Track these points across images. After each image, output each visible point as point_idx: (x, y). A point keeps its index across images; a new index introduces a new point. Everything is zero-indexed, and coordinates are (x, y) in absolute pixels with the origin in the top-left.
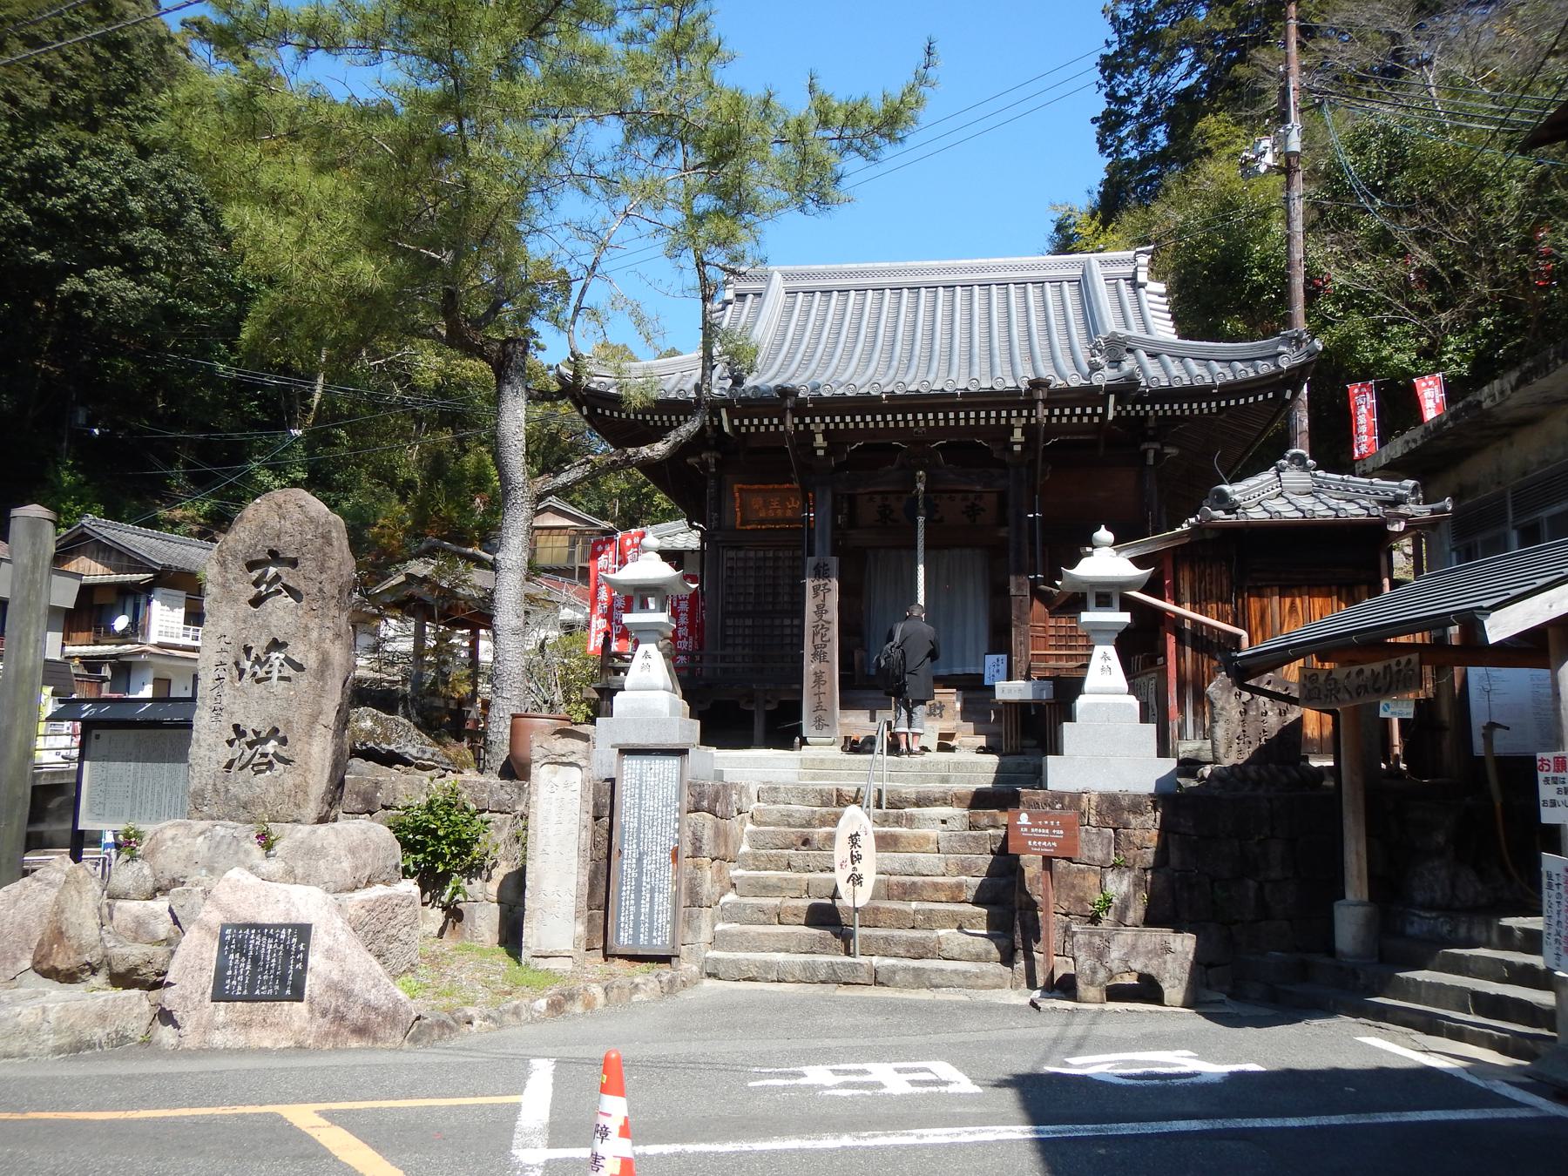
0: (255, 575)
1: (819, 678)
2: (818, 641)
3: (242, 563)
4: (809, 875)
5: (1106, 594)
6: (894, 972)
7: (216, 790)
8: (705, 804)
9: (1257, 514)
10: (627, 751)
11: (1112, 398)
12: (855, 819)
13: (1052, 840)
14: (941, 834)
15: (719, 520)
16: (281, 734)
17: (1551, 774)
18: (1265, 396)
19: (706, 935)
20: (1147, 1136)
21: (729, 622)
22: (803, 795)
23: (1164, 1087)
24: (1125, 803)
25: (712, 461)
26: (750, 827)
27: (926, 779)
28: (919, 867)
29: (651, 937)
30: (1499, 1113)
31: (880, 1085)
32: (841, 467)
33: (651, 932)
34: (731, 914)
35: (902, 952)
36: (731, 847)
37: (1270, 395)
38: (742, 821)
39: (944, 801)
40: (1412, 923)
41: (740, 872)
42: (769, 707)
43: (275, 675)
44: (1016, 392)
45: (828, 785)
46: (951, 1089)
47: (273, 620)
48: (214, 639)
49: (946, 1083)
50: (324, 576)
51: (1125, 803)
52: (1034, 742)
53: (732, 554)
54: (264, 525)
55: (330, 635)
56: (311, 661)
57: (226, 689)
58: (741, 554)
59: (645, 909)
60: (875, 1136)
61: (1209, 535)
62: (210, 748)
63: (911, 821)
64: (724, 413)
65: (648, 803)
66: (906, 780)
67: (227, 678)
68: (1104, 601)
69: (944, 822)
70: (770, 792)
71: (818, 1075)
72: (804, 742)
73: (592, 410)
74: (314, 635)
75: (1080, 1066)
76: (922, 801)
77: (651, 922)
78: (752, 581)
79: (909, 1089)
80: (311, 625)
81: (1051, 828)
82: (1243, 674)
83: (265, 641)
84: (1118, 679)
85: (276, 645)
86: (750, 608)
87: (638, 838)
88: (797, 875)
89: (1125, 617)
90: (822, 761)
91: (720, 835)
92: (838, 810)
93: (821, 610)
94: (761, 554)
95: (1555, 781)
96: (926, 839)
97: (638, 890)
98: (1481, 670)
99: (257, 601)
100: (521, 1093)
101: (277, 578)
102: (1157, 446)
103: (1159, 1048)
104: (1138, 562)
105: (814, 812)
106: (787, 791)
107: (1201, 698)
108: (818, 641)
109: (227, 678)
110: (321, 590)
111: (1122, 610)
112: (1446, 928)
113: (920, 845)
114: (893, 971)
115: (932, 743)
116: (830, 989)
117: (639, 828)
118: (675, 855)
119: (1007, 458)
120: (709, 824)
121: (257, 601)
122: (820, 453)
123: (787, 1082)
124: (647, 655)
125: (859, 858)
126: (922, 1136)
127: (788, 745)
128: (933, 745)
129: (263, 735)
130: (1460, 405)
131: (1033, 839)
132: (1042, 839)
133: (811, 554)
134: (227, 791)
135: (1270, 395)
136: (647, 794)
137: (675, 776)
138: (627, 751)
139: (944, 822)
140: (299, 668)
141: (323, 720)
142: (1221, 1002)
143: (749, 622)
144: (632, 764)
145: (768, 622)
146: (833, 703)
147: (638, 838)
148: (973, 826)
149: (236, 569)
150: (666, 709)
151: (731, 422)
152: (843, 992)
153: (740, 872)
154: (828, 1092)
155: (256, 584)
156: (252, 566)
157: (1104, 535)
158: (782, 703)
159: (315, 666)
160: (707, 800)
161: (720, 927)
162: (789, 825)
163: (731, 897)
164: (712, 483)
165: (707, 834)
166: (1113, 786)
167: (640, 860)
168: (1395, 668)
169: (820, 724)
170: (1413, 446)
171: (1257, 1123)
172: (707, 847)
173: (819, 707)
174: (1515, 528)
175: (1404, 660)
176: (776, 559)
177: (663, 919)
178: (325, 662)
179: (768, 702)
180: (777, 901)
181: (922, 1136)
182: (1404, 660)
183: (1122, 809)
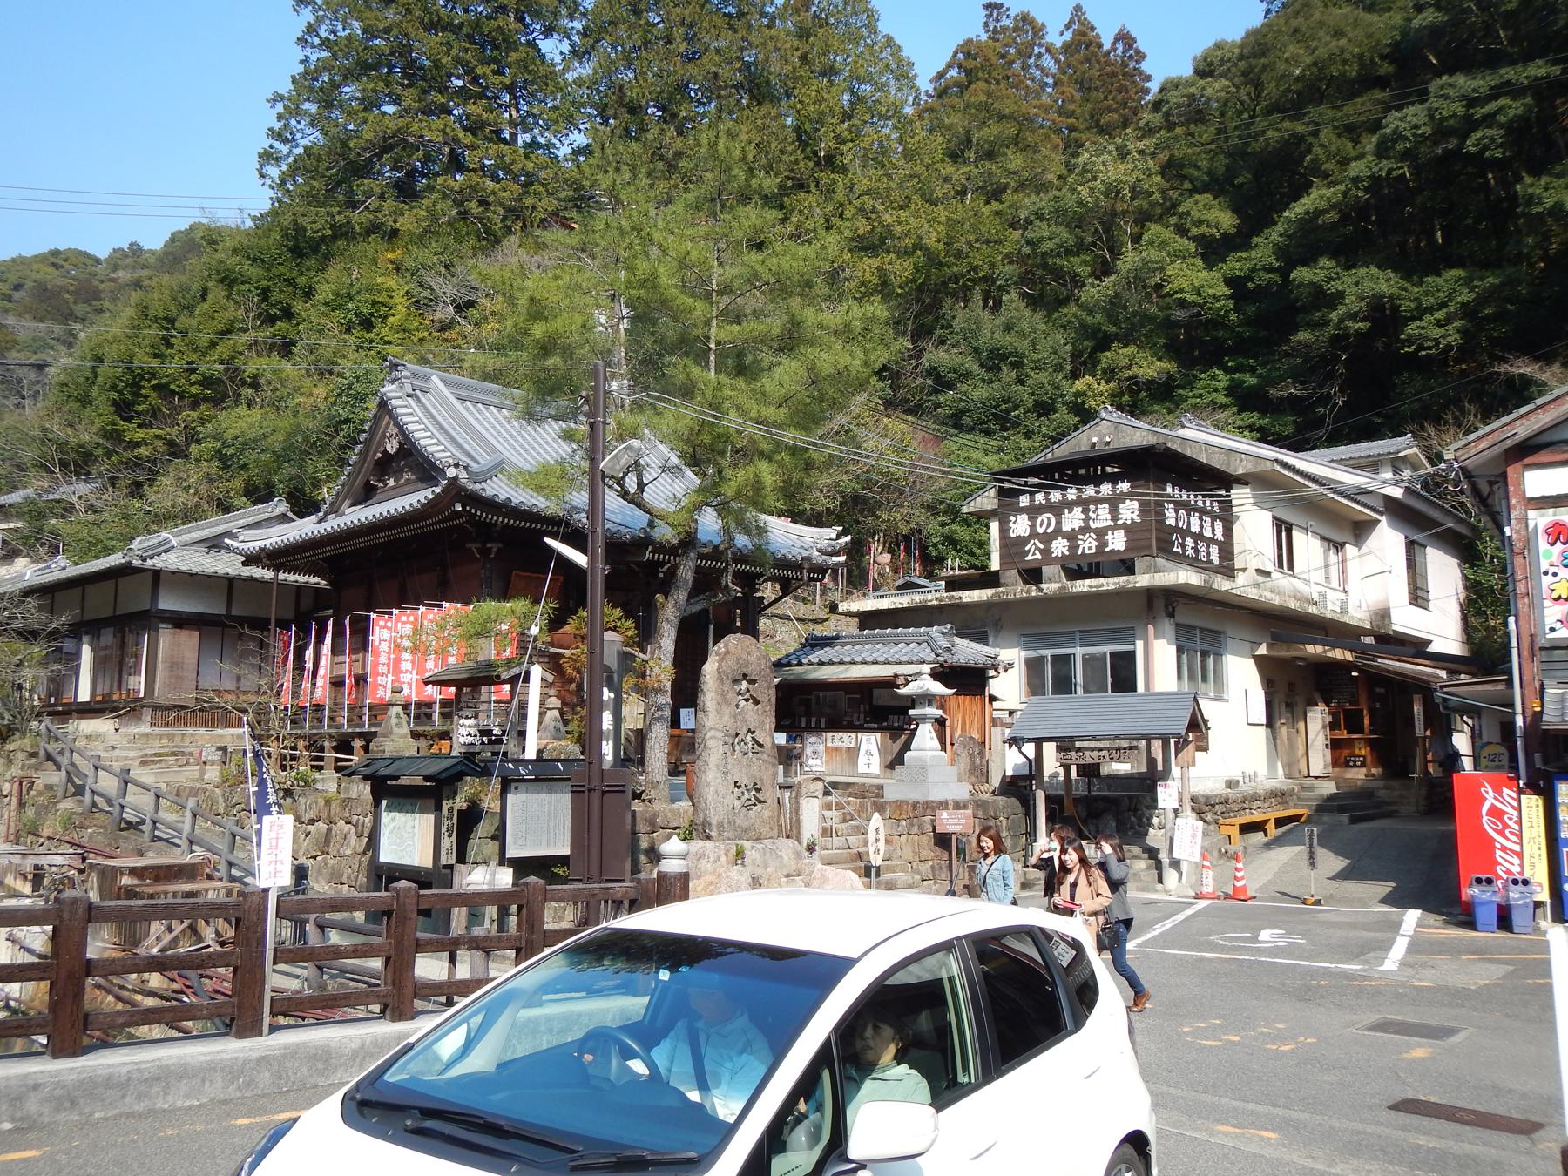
140: (761, 745)
149: (728, 683)
156: (735, 682)
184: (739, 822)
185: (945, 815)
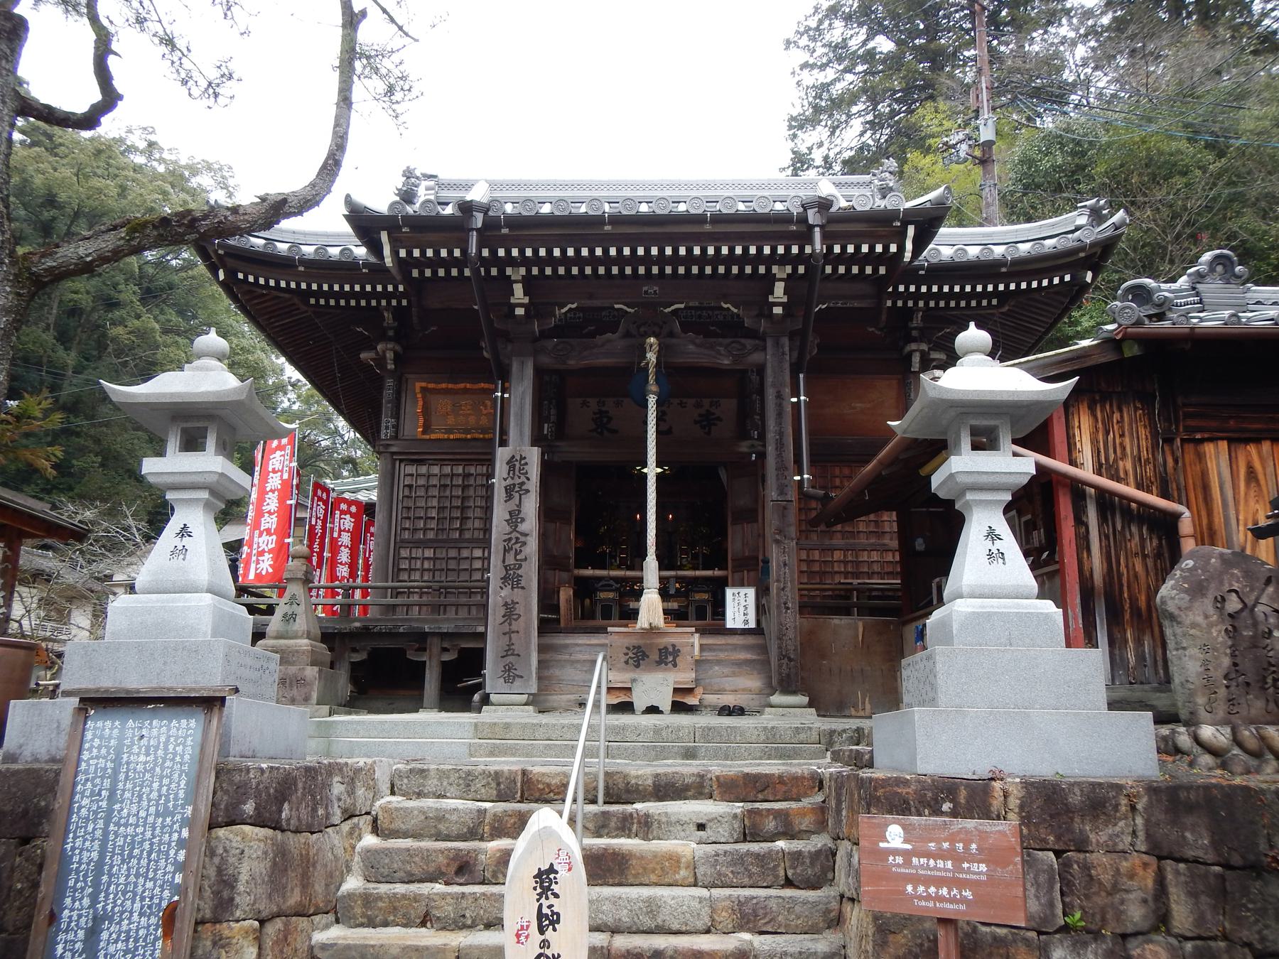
1: (510, 610)
2: (510, 560)
5: (985, 422)
10: (101, 702)
11: (911, 230)
12: (552, 834)
13: (961, 884)
15: (396, 427)
18: (1062, 279)
21: (404, 553)
22: (467, 783)
24: (1076, 799)
25: (390, 355)
27: (661, 754)
28: (664, 917)
32: (545, 335)
36: (319, 888)
37: (1067, 278)
38: (355, 834)
39: (697, 789)
42: (447, 657)
44: (784, 218)
45: (508, 764)
51: (1076, 799)
52: (805, 700)
53: (411, 469)
58: (423, 470)
61: (1131, 351)
63: (645, 826)
64: (384, 236)
65: (126, 809)
66: (632, 756)
68: (984, 441)
69: (701, 827)
70: (412, 780)
72: (486, 700)
73: (231, 274)
76: (666, 790)
78: (435, 503)
84: (1018, 571)
86: (431, 535)
87: (96, 884)
90: (507, 726)
92: (523, 807)
93: (515, 518)
94: (447, 470)
100: (515, 838)
102: (924, 347)
105: (482, 812)
106: (443, 775)
108: (510, 560)
113: (664, 871)
117: (100, 864)
118: (170, 918)
119: (763, 325)
122: (520, 311)
124: (184, 532)
125: (554, 920)
127: (466, 706)
128: (666, 705)
131: (916, 880)
132: (939, 882)
133: (503, 443)
135: (1067, 278)
138: (101, 702)
139: (701, 827)
143: (429, 553)
145: (453, 553)
146: (528, 643)
147: (96, 884)
148: (748, 835)
150: (205, 625)
151: (395, 253)
157: (972, 325)
158: (462, 651)
162: (439, 837)
164: (390, 382)
166: (1044, 768)
167: (93, 934)
169: (510, 674)
173: (509, 651)
176: (466, 476)
179: (445, 650)
183: (1069, 810)
185: (895, 836)
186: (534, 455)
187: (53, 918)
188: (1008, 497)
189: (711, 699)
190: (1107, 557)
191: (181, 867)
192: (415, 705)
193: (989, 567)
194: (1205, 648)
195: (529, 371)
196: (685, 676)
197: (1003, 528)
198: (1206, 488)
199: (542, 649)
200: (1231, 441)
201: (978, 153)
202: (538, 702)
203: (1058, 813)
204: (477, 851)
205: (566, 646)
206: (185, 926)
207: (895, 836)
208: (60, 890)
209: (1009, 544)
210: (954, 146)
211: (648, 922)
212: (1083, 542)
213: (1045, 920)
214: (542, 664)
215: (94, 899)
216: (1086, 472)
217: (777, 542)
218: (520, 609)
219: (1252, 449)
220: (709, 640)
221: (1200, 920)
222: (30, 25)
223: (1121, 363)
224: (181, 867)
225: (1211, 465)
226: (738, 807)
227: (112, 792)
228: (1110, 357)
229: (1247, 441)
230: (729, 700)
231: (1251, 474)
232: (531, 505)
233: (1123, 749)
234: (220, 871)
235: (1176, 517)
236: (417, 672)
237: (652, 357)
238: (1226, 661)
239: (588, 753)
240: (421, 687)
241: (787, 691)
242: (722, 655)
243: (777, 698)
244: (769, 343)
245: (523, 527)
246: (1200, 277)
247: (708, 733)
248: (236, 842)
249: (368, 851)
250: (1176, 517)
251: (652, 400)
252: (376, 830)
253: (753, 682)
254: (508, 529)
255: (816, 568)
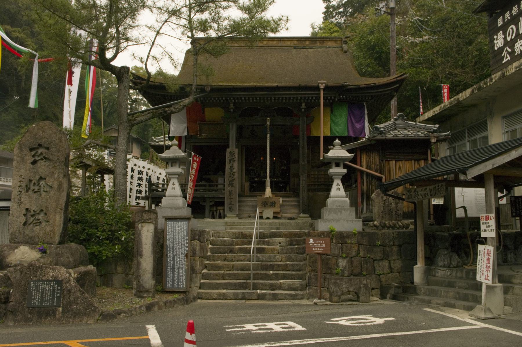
0: (33, 153)
1: (231, 193)
2: (231, 179)
3: (28, 149)
4: (232, 263)
6: (266, 295)
7: (20, 233)
8: (197, 237)
9: (390, 135)
10: (168, 219)
13: (321, 248)
14: (279, 248)
16: (44, 212)
17: (484, 221)
19: (198, 285)
20: (363, 339)
23: (365, 326)
26: (210, 246)
27: (272, 229)
29: (178, 285)
30: (469, 327)
31: (271, 329)
33: (178, 283)
34: (205, 276)
35: (268, 288)
40: (438, 272)
41: (207, 262)
43: (42, 190)
46: (296, 329)
47: (40, 170)
48: (18, 177)
49: (294, 328)
50: (60, 154)
52: (308, 215)
54: (36, 135)
55: (62, 175)
56: (56, 185)
57: (23, 196)
59: (176, 275)
60: (275, 343)
61: (373, 142)
62: (17, 217)
63: (268, 243)
67: (23, 191)
68: (337, 165)
69: (280, 243)
71: (249, 327)
74: (56, 175)
75: (336, 321)
77: (178, 280)
79: (282, 330)
80: (55, 172)
81: (321, 244)
82: (385, 189)
83: (37, 177)
85: (41, 178)
87: (173, 250)
88: (229, 263)
89: (345, 171)
90: (234, 222)
91: (202, 248)
93: (232, 168)
95: (486, 223)
96: (274, 249)
97: (173, 269)
98: (460, 189)
99: (34, 163)
101: (41, 154)
103: (360, 314)
104: (349, 151)
107: (369, 198)
108: (231, 179)
109: (23, 191)
110: (58, 159)
111: (344, 168)
112: (449, 273)
114: (265, 295)
115: (271, 215)
116: (243, 301)
117: (173, 246)
118: (187, 256)
120: (198, 245)
121: (34, 163)
123: (240, 329)
124: (174, 184)
126: (291, 343)
128: (271, 217)
129: (37, 212)
130: (452, 99)
131: (314, 248)
132: (318, 248)
134: (24, 233)
136: (176, 234)
137: (186, 228)
138: (168, 219)
139: (280, 243)
141: (60, 207)
142: (377, 300)
144: (170, 224)
147: (173, 250)
149: (26, 151)
152: (248, 302)
153: (207, 262)
154: (255, 332)
155: (33, 156)
156: (31, 150)
159: (56, 187)
160: (196, 236)
161: (202, 281)
162: (224, 245)
163: (205, 271)
165: (198, 248)
167: (174, 258)
168: (437, 188)
169: (231, 210)
170: (436, 113)
171: (397, 334)
172: (198, 252)
173: (231, 203)
174: (469, 141)
175: (440, 185)
177: (183, 278)
178: (60, 186)
179: (211, 202)
180: (223, 272)
181: (291, 343)
182: (440, 185)
184: (27, 232)
186: (236, 151)
187: (167, 255)
188: (341, 177)
189: (284, 215)
190: (367, 186)
191: (187, 247)
192: (203, 217)
193: (338, 191)
194: (379, 207)
195: (235, 128)
196: (277, 209)
197: (340, 183)
198: (390, 171)
199: (239, 202)
200: (396, 161)
201: (389, 11)
202: (239, 217)
203: (341, 237)
204: (233, 248)
205: (245, 201)
206: (189, 256)
207: (311, 241)
208: (167, 251)
209: (341, 186)
210: (379, 10)
211: (269, 260)
212: (362, 183)
213: (338, 255)
214: (239, 206)
215: (173, 252)
216: (364, 169)
217: (302, 174)
218: (233, 193)
219: (400, 162)
220: (285, 199)
221: (364, 254)
222: (124, 65)
223: (370, 145)
224: (187, 247)
225: (391, 166)
226: (288, 239)
227: (173, 234)
228: (369, 143)
229: (399, 160)
230: (289, 215)
231: (400, 168)
232: (236, 165)
233: (357, 226)
234: (193, 248)
235: (382, 178)
236: (204, 208)
237: (268, 123)
238: (382, 209)
239: (256, 229)
240: (205, 212)
241: (304, 213)
242: (288, 203)
243: (302, 215)
244: (301, 119)
245: (234, 171)
246: (396, 120)
247: (283, 224)
248: (195, 243)
249: (211, 248)
250: (382, 178)
251: (268, 136)
252: (211, 244)
253: (296, 211)
254: (230, 171)
255: (316, 176)
